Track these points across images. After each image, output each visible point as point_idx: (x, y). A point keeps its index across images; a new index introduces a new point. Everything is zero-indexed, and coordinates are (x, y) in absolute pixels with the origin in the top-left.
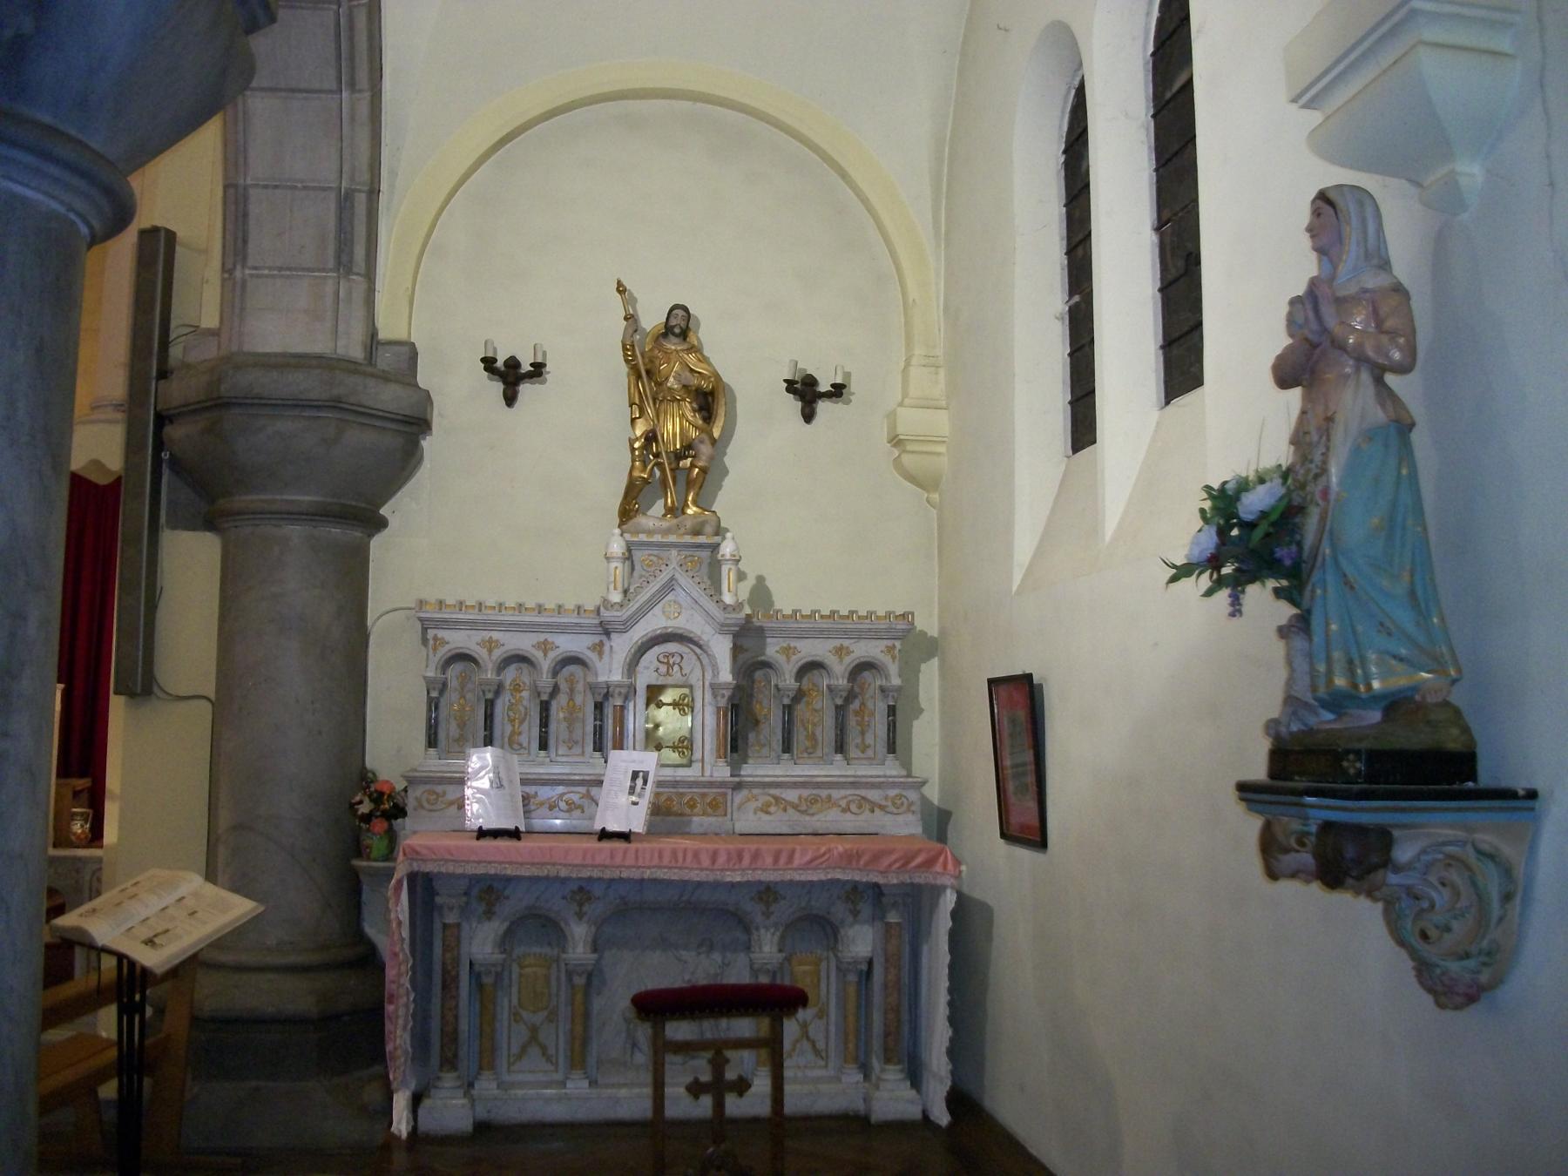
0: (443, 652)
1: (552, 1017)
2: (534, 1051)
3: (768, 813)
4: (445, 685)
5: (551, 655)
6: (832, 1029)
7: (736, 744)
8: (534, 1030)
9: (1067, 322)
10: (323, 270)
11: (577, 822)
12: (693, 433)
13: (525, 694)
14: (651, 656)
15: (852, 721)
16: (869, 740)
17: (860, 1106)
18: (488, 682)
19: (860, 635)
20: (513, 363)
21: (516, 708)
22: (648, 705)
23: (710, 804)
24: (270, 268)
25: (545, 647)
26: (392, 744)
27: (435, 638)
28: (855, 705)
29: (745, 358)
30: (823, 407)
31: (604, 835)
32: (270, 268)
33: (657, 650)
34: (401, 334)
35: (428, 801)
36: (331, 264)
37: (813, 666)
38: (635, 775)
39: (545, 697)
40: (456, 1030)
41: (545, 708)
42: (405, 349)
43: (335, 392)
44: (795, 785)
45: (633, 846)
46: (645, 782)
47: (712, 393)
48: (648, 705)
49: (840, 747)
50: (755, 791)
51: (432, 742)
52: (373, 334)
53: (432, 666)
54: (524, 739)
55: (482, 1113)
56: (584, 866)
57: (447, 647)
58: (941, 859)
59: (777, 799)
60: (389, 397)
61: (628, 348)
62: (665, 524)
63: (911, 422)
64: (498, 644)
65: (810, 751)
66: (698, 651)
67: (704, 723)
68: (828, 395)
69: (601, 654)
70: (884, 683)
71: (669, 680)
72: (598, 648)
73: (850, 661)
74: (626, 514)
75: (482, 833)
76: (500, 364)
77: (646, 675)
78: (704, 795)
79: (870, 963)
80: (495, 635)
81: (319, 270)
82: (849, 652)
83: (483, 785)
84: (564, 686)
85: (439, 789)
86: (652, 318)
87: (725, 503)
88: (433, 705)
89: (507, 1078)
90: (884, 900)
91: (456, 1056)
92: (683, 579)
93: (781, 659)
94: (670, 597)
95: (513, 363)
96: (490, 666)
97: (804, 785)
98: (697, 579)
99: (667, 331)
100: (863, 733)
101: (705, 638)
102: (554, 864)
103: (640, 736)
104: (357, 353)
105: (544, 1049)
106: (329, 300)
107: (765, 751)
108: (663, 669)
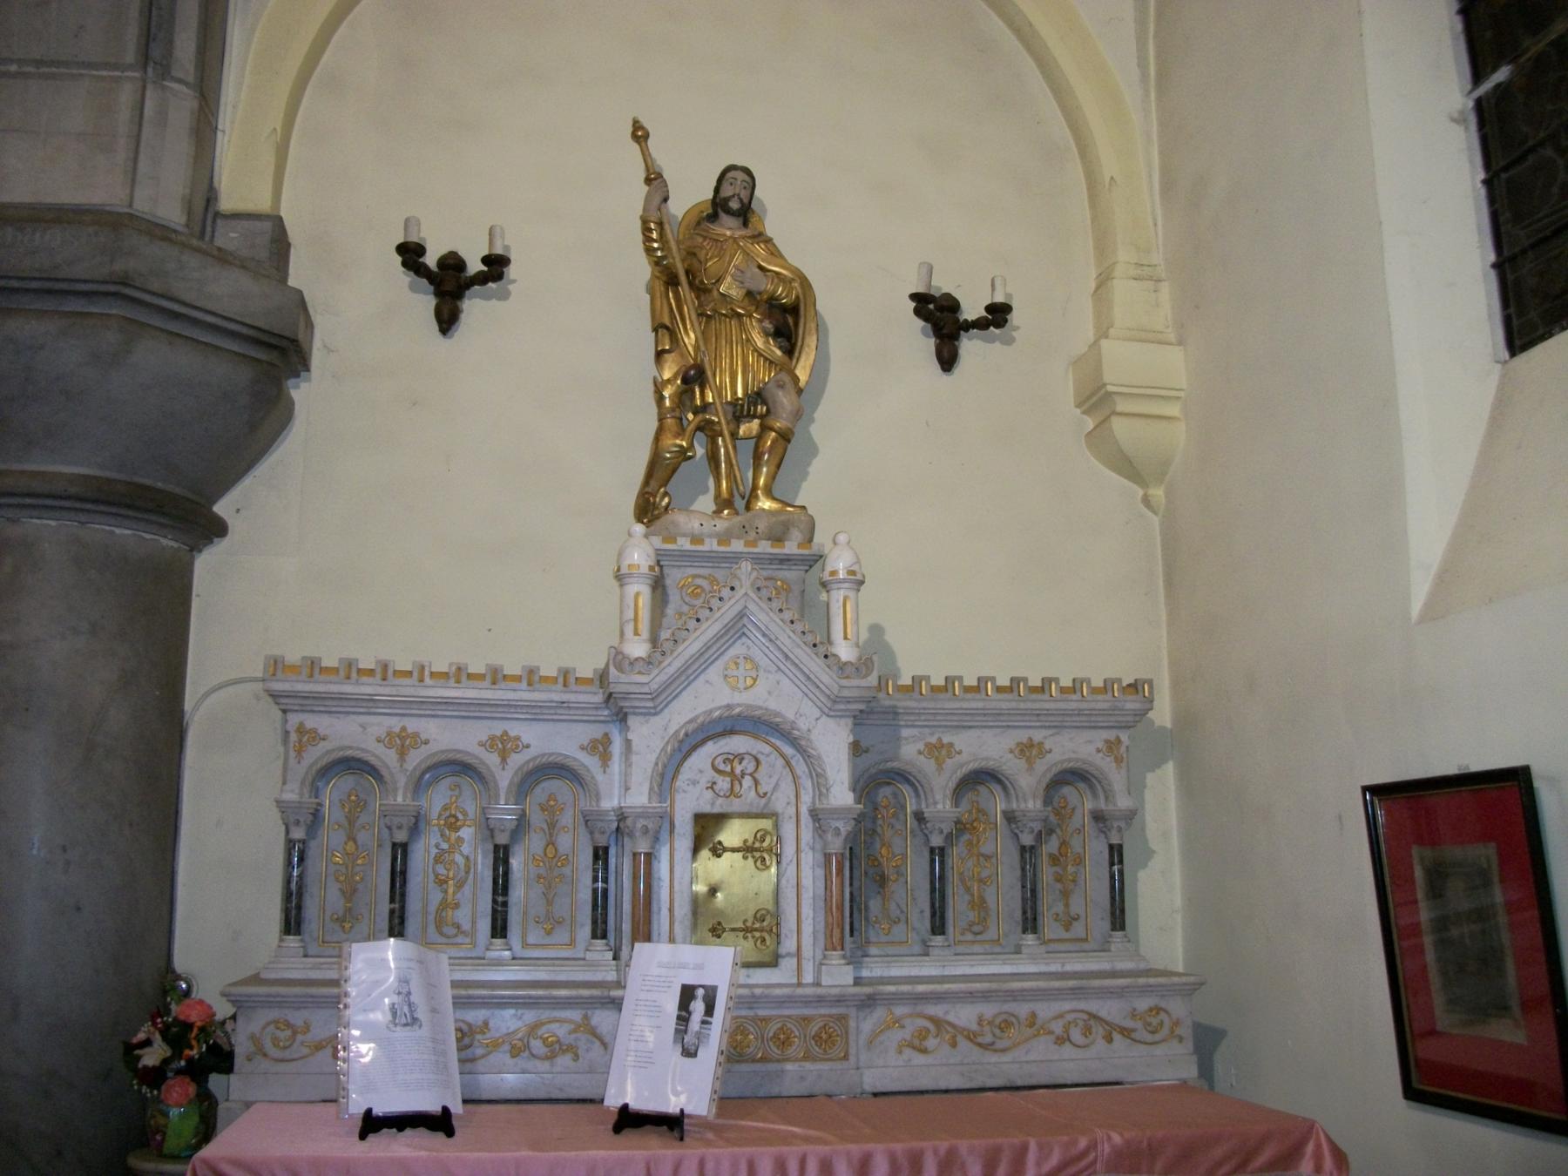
0: (315, 755)
3: (924, 1051)
4: (316, 815)
5: (516, 760)
7: (851, 924)
9: (1473, 126)
10: (115, 67)
11: (563, 1077)
12: (765, 375)
13: (466, 833)
14: (701, 760)
15: (1047, 873)
16: (1076, 906)
19: (1060, 722)
20: (452, 263)
21: (452, 858)
22: (696, 850)
23: (817, 1038)
24: (20, 62)
25: (504, 746)
26: (220, 927)
27: (301, 730)
28: (1052, 846)
29: (849, 248)
30: (970, 346)
31: (628, 1120)
32: (20, 62)
33: (711, 749)
34: (260, 202)
35: (275, 1042)
36: (130, 57)
37: (980, 778)
38: (687, 993)
39: (502, 839)
41: (501, 856)
42: (267, 226)
43: (119, 266)
44: (971, 997)
45: (690, 1152)
46: (709, 1010)
47: (794, 310)
48: (696, 850)
49: (1030, 923)
50: (899, 1010)
51: (292, 923)
52: (211, 197)
54: (462, 916)
57: (323, 746)
59: (936, 1021)
60: (229, 293)
61: (653, 225)
62: (721, 525)
63: (1124, 363)
64: (417, 740)
65: (977, 928)
66: (789, 750)
67: (801, 882)
68: (981, 324)
69: (605, 758)
70: (1102, 805)
71: (736, 805)
72: (600, 748)
73: (1045, 767)
74: (646, 511)
75: (372, 1124)
76: (431, 260)
77: (691, 799)
78: (807, 1020)
80: (412, 725)
81: (106, 66)
82: (1042, 751)
83: (383, 1021)
84: (537, 818)
85: (297, 1018)
86: (690, 192)
87: (817, 489)
88: (296, 853)
92: (761, 615)
93: (927, 765)
94: (738, 649)
95: (452, 263)
96: (402, 781)
97: (986, 996)
98: (787, 615)
99: (718, 206)
100: (1066, 894)
101: (803, 725)
103: (683, 910)
104: (172, 213)
106: (124, 115)
107: (899, 931)
108: (723, 784)
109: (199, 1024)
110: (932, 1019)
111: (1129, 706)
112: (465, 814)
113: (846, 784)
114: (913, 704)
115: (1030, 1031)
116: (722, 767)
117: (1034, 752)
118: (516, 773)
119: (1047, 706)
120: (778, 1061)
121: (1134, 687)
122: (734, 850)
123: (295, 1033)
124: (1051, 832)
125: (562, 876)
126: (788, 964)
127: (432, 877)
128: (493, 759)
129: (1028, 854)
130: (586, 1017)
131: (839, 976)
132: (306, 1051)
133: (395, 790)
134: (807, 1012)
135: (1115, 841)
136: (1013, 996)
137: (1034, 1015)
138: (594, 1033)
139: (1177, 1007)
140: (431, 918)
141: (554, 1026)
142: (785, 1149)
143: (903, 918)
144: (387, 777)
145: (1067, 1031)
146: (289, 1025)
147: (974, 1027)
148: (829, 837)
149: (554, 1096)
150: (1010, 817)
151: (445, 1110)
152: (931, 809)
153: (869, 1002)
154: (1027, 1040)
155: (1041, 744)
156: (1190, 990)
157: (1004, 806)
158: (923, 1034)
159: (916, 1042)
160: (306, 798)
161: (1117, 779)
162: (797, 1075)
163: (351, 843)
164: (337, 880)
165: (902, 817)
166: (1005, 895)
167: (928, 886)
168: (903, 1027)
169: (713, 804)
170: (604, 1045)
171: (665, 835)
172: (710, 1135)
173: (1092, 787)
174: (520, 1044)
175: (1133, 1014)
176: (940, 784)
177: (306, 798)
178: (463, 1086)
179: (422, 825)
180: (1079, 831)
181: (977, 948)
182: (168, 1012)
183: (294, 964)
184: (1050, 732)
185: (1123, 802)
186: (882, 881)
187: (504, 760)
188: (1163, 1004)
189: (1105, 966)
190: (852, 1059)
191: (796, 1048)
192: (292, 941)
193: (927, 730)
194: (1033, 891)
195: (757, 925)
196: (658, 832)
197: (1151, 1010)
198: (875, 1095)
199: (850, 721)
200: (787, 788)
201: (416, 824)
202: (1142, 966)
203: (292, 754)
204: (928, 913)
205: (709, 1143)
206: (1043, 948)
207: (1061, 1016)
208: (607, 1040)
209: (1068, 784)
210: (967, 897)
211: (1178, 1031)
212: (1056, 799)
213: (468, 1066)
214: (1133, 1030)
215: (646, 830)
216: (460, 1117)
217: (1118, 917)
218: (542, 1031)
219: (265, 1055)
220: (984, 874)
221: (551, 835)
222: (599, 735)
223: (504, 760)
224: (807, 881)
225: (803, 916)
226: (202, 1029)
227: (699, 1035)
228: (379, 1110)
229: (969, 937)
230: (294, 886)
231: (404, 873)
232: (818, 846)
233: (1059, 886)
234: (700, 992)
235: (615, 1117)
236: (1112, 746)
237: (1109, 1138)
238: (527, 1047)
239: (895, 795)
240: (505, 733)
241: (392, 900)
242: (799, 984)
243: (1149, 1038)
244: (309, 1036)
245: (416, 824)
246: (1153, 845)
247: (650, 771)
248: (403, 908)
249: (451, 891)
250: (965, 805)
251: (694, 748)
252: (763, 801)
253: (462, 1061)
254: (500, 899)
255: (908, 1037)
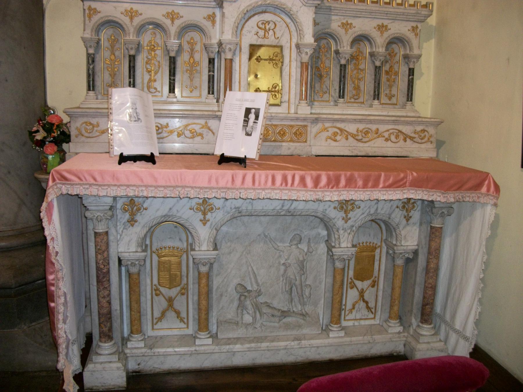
0: (96, 19)
1: (184, 291)
2: (171, 314)
3: (336, 141)
4: (98, 42)
5: (178, 22)
6: (380, 293)
8: (170, 301)
13: (158, 52)
15: (384, 78)
16: (394, 91)
17: (400, 349)
18: (131, 42)
22: (250, 59)
23: (295, 133)
26: (64, 87)
27: (90, 8)
28: (386, 67)
31: (224, 160)
33: (256, 18)
35: (86, 130)
37: (361, 39)
38: (248, 111)
39: (172, 54)
40: (110, 313)
44: (355, 121)
46: (257, 118)
50: (327, 125)
51: (91, 86)
53: (88, 31)
54: (157, 85)
55: (132, 366)
56: (211, 188)
57: (99, 16)
58: (486, 182)
59: (341, 130)
65: (356, 97)
66: (288, 20)
69: (214, 22)
71: (266, 42)
72: (211, 18)
75: (123, 159)
77: (249, 37)
78: (292, 126)
79: (416, 253)
83: (126, 119)
84: (186, 47)
88: (91, 59)
89: (150, 333)
90: (434, 210)
91: (110, 329)
93: (341, 32)
96: (132, 30)
97: (361, 121)
100: (390, 87)
101: (294, 9)
102: (184, 187)
105: (178, 313)
108: (261, 33)
109: (56, 124)
110: (339, 129)
111: (423, 13)
112: (158, 45)
113: (311, 35)
114: (338, 6)
115: (376, 136)
116: (261, 26)
117: (384, 29)
118: (178, 28)
119: (391, 10)
120: (280, 142)
121: (426, 6)
122: (265, 60)
123: (93, 127)
124: (387, 62)
125: (196, 70)
126: (285, 105)
127: (145, 69)
128: (168, 22)
129: (377, 70)
130: (206, 123)
131: (305, 110)
132: (98, 134)
133: (129, 34)
134: (292, 123)
135: (411, 67)
136: (371, 122)
137: (378, 129)
138: (209, 129)
139: (431, 130)
140: (145, 85)
141: (194, 126)
142: (287, 172)
143: (328, 92)
144: (126, 29)
145: (390, 137)
146: (91, 124)
147: (355, 133)
148: (303, 55)
149: (194, 152)
150: (372, 55)
151: (152, 154)
152: (342, 49)
153: (316, 121)
154: (374, 139)
155: (387, 26)
156: (437, 124)
157: (369, 51)
158: (335, 134)
159: (333, 137)
160: (94, 37)
161: (415, 42)
162: (287, 148)
163: (113, 56)
164: (108, 70)
165: (330, 52)
166: (367, 84)
167: (338, 80)
168: (328, 131)
169: (257, 41)
170: (213, 133)
171: (237, 52)
172: (256, 166)
173: (404, 46)
174: (181, 132)
175: (415, 132)
176: (346, 39)
177: (94, 37)
178: (159, 148)
179: (140, 49)
180: (398, 62)
181: (355, 105)
182: (45, 120)
183: (93, 102)
184: (392, 21)
185: (416, 52)
186: (321, 77)
187: (173, 22)
188: (426, 129)
189: (404, 114)
190: (308, 142)
191: (287, 137)
192: (91, 93)
193: (342, 17)
194: (379, 84)
195: (273, 90)
196: (235, 50)
197: (422, 131)
198: (316, 156)
199: (314, 8)
200: (287, 36)
201: (138, 48)
202: (418, 115)
203: (87, 19)
204: (338, 91)
205: (256, 169)
206: (381, 106)
207: (388, 131)
208: (214, 131)
209: (395, 43)
210: (353, 85)
211: (431, 139)
212: (390, 49)
213: (161, 140)
214: (415, 138)
215: (230, 50)
216: (157, 157)
217: (410, 96)
218: (189, 127)
219: (83, 135)
220: (360, 76)
221: (192, 54)
222: (211, 13)
223: (173, 22)
224: (293, 73)
225: (291, 87)
226: (58, 126)
227: (252, 127)
228: (125, 154)
229: (353, 100)
230: (91, 72)
231: (134, 67)
232: (299, 59)
233: (388, 83)
234: (253, 111)
235: (219, 158)
236: (414, 29)
237: (412, 174)
238: (183, 133)
239: (327, 43)
240: (173, 11)
241: (130, 78)
242: (289, 113)
243: (420, 141)
244: (99, 129)
245: (138, 48)
246: (423, 71)
247: (232, 25)
248: (134, 81)
249: (153, 75)
250: (354, 49)
251: (250, 18)
252: (277, 40)
253: (158, 138)
254: (172, 78)
255: (330, 135)
